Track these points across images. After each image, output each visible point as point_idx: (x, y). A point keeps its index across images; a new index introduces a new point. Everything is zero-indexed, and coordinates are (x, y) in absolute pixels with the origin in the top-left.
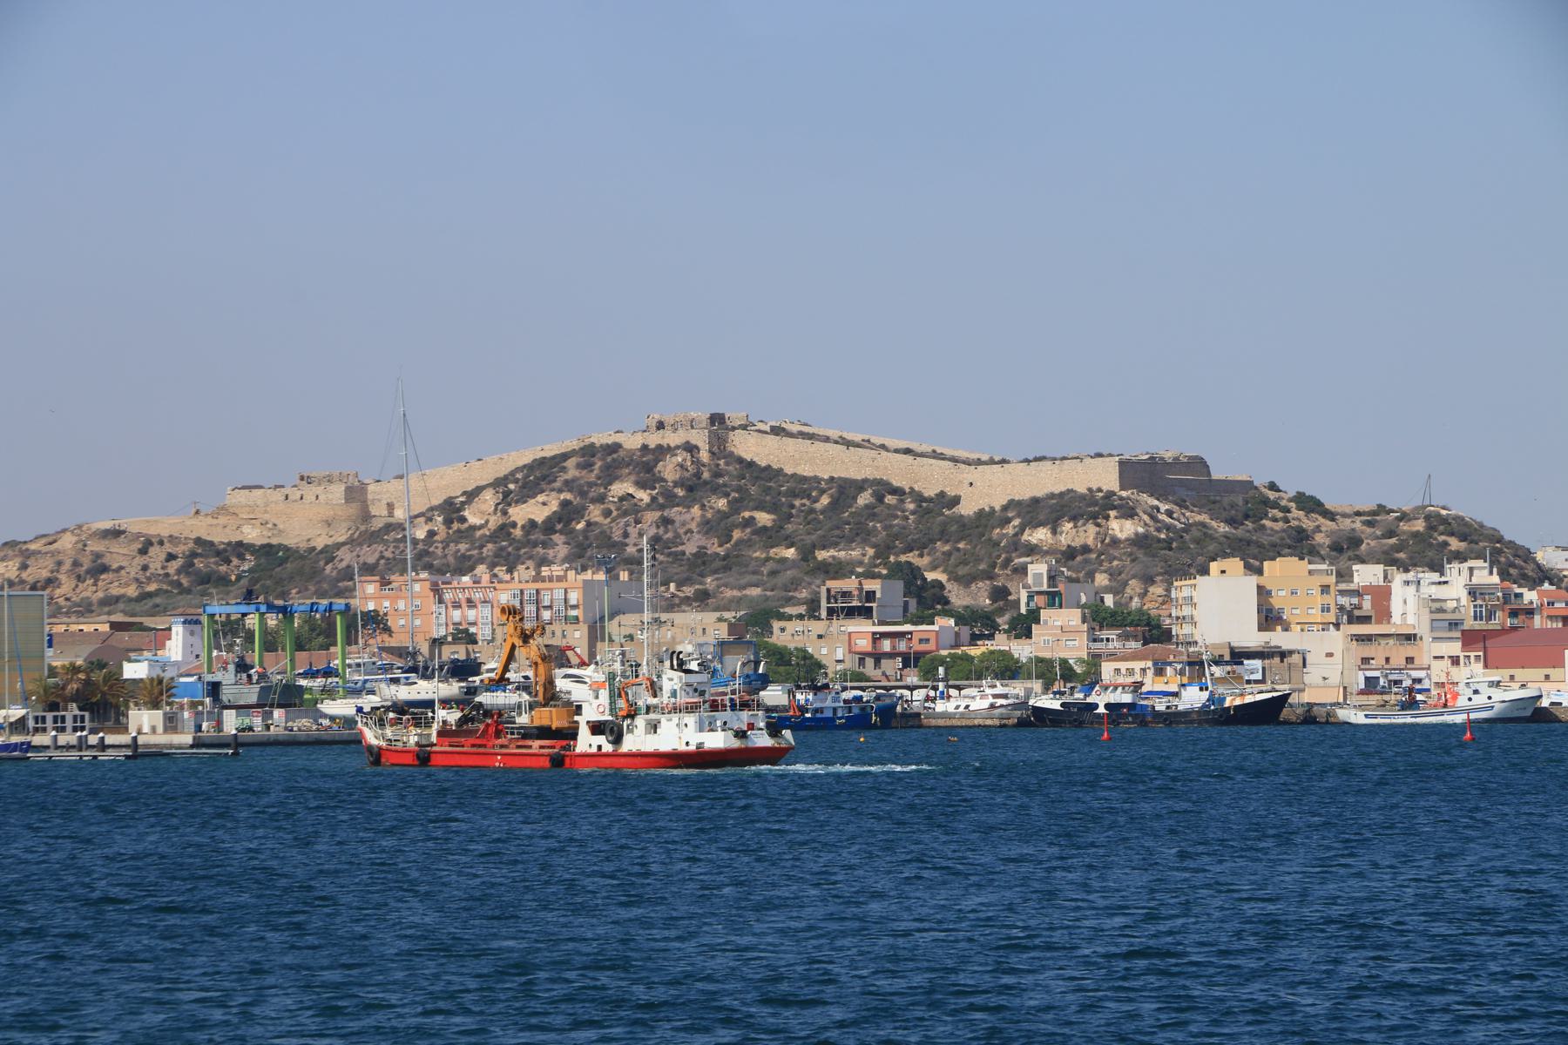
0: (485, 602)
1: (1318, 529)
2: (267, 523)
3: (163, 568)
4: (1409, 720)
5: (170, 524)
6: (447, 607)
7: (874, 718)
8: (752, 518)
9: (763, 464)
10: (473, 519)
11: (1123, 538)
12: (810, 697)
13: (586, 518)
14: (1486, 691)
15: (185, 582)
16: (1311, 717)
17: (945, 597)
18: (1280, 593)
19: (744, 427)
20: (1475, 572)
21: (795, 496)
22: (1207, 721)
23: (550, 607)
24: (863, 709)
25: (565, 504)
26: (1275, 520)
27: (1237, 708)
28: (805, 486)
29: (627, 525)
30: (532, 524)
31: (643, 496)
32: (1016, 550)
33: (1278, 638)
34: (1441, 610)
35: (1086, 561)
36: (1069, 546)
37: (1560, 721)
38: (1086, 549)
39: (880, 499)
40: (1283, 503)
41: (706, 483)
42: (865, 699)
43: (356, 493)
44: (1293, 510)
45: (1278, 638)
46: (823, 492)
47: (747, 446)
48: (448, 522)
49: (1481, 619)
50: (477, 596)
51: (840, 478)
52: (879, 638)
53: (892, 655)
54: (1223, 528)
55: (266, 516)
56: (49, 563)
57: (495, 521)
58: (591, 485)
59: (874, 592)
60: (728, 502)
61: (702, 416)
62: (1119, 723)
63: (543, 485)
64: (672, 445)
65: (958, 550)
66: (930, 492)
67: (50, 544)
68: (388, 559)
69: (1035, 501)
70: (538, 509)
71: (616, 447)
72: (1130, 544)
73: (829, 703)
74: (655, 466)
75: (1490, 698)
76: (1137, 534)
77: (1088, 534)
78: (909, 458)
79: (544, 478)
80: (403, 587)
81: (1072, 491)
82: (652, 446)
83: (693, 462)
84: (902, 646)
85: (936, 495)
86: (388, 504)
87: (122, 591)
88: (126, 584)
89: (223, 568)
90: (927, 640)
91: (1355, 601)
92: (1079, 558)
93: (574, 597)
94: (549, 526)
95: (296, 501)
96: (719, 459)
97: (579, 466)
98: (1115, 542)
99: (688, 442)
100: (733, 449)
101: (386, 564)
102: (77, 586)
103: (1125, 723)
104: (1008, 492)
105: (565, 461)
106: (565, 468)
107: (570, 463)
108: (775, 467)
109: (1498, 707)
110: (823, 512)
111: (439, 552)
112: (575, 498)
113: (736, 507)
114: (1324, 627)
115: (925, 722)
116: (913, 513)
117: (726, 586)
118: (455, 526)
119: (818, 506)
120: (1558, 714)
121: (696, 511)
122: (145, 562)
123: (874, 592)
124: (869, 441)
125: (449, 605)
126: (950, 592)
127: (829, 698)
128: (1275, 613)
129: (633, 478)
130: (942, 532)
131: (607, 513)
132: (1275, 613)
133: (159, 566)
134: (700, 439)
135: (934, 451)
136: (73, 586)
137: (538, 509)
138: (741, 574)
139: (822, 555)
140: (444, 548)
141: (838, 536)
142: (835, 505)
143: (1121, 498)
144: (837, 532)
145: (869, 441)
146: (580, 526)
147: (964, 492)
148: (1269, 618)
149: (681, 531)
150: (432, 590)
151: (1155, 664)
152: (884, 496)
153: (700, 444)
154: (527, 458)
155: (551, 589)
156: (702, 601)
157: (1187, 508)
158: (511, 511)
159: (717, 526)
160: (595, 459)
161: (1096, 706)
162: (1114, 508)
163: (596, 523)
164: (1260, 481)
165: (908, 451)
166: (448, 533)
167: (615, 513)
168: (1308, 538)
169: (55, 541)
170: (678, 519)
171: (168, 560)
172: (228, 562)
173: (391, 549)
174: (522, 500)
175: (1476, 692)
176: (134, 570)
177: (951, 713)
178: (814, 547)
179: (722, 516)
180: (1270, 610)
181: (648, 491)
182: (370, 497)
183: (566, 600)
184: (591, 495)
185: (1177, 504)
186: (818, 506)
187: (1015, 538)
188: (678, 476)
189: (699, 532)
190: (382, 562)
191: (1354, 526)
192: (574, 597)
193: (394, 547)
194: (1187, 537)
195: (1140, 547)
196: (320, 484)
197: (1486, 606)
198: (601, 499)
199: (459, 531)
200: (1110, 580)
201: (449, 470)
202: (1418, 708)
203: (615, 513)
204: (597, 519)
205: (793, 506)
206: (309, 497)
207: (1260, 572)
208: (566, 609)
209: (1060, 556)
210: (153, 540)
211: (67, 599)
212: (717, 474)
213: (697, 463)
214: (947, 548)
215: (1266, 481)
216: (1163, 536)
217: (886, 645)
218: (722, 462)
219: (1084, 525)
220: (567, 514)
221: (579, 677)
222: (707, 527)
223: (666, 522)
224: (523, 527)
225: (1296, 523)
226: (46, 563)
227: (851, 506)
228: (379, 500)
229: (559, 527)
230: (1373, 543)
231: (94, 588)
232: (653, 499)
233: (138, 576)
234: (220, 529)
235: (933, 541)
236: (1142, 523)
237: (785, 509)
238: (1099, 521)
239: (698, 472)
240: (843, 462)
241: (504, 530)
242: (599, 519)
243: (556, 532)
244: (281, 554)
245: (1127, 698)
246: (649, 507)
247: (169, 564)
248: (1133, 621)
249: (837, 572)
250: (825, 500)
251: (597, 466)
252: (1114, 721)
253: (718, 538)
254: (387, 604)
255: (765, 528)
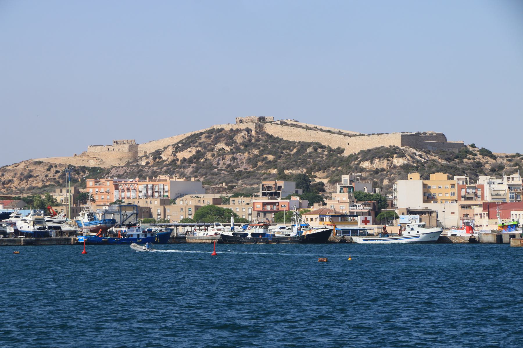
0: (134, 189)
1: (487, 163)
2: (99, 159)
3: (54, 176)
4: (382, 242)
5: (62, 160)
6: (119, 191)
7: (156, 239)
8: (266, 158)
9: (276, 136)
10: (164, 158)
11: (398, 165)
12: (127, 229)
13: (205, 157)
14: (416, 229)
15: (61, 181)
16: (344, 240)
17: (323, 189)
18: (434, 187)
19: (271, 122)
20: (514, 179)
21: (284, 149)
22: (295, 242)
23: (158, 192)
24: (152, 235)
25: (198, 152)
26: (469, 159)
27: (307, 235)
28: (290, 145)
29: (219, 160)
30: (184, 159)
31: (228, 149)
32: (356, 170)
33: (431, 206)
34: (497, 195)
35: (382, 175)
36: (377, 169)
37: (452, 243)
38: (383, 170)
39: (316, 150)
40: (475, 152)
41: (252, 144)
42: (153, 231)
43: (133, 148)
44: (478, 155)
45: (431, 206)
46: (295, 147)
47: (271, 130)
48: (154, 159)
49: (513, 198)
50: (132, 187)
51: (303, 142)
52: (266, 205)
53: (270, 212)
54: (444, 162)
55: (99, 157)
56: (12, 174)
57: (171, 159)
58: (209, 144)
59: (281, 186)
60: (259, 151)
61: (256, 118)
62: (257, 242)
63: (191, 144)
64: (242, 129)
65: (337, 170)
66: (334, 147)
67: (16, 167)
68: (128, 173)
69: (369, 151)
70: (187, 154)
71: (223, 129)
72: (401, 168)
73: (135, 232)
74: (234, 137)
75: (418, 232)
76: (404, 164)
77: (383, 164)
78: (328, 134)
79: (192, 141)
80: (104, 183)
81: (384, 147)
82: (234, 129)
83: (248, 136)
84: (275, 208)
85: (337, 148)
86: (145, 152)
87: (37, 185)
88: (39, 182)
89: (76, 176)
90: (285, 206)
91: (474, 191)
92: (380, 173)
93: (167, 188)
94: (190, 161)
95: (111, 151)
96: (259, 134)
97: (206, 137)
98: (395, 167)
99: (247, 128)
100: (265, 130)
101: (126, 175)
102: (20, 183)
103: (259, 242)
104: (362, 147)
105: (201, 135)
106: (201, 138)
107: (203, 136)
108: (280, 138)
109: (422, 236)
110: (293, 155)
111: (146, 170)
112: (202, 149)
113: (262, 153)
114: (452, 201)
115: (187, 241)
116: (326, 155)
117: (245, 184)
118: (157, 160)
119: (292, 153)
120: (451, 239)
121: (246, 155)
122: (47, 174)
123: (281, 186)
124: (316, 127)
125: (120, 191)
126: (326, 187)
127: (135, 230)
128: (432, 196)
129: (225, 141)
130: (333, 163)
131: (213, 155)
132: (432, 196)
133: (52, 176)
134: (252, 126)
135: (340, 131)
136: (19, 183)
137: (187, 154)
138: (252, 179)
139: (287, 172)
140: (148, 169)
141: (294, 165)
142: (298, 152)
143: (400, 150)
144: (294, 163)
145: (316, 127)
146: (202, 160)
147: (346, 147)
148: (428, 197)
149: (239, 163)
150: (114, 184)
151: (320, 216)
152: (317, 149)
153: (252, 129)
154: (189, 134)
155: (158, 184)
156: (230, 190)
157: (429, 154)
158: (177, 154)
159: (253, 161)
160: (213, 135)
161: (247, 234)
162: (396, 153)
163: (209, 159)
164: (467, 143)
165: (329, 131)
166: (154, 163)
167: (216, 155)
168: (482, 166)
169: (18, 166)
170: (239, 158)
171: (56, 173)
172: (79, 174)
173: (129, 169)
174: (182, 150)
175: (412, 229)
176: (42, 177)
177: (201, 237)
178: (284, 169)
179: (256, 156)
180: (430, 195)
181: (230, 147)
182: (139, 149)
183: (163, 189)
184: (209, 148)
185: (425, 152)
186: (292, 153)
187: (357, 165)
188: (242, 141)
189: (246, 163)
190: (125, 174)
191: (503, 161)
192: (167, 188)
193: (131, 168)
194: (426, 165)
195: (404, 169)
196: (121, 145)
197: (515, 193)
198: (212, 150)
199: (158, 162)
200: (389, 182)
201: (166, 139)
202: (388, 236)
203: (216, 155)
204: (209, 158)
205: (282, 153)
206: (116, 150)
207: (428, 178)
208: (163, 192)
209: (372, 172)
210: (53, 165)
211: (16, 188)
212: (258, 140)
213: (251, 136)
214: (334, 169)
215: (471, 143)
216: (415, 165)
217: (268, 208)
218: (260, 136)
219: (383, 160)
220: (199, 155)
221: (26, 220)
222: (249, 161)
223: (234, 159)
224: (181, 161)
225: (478, 160)
226: (11, 174)
227: (304, 153)
228: (142, 151)
229: (195, 161)
230: (508, 168)
231: (27, 184)
232: (231, 150)
233: (43, 179)
234: (81, 162)
235: (329, 167)
236: (407, 159)
237: (279, 154)
238: (389, 158)
239: (250, 139)
240: (304, 135)
241: (174, 161)
242: (210, 158)
243: (193, 163)
244: (98, 171)
245: (261, 231)
246: (229, 153)
247: (56, 175)
248: (374, 198)
249: (288, 179)
250: (295, 150)
251: (213, 137)
252: (254, 241)
253: (252, 165)
254: (97, 190)
255: (270, 161)
